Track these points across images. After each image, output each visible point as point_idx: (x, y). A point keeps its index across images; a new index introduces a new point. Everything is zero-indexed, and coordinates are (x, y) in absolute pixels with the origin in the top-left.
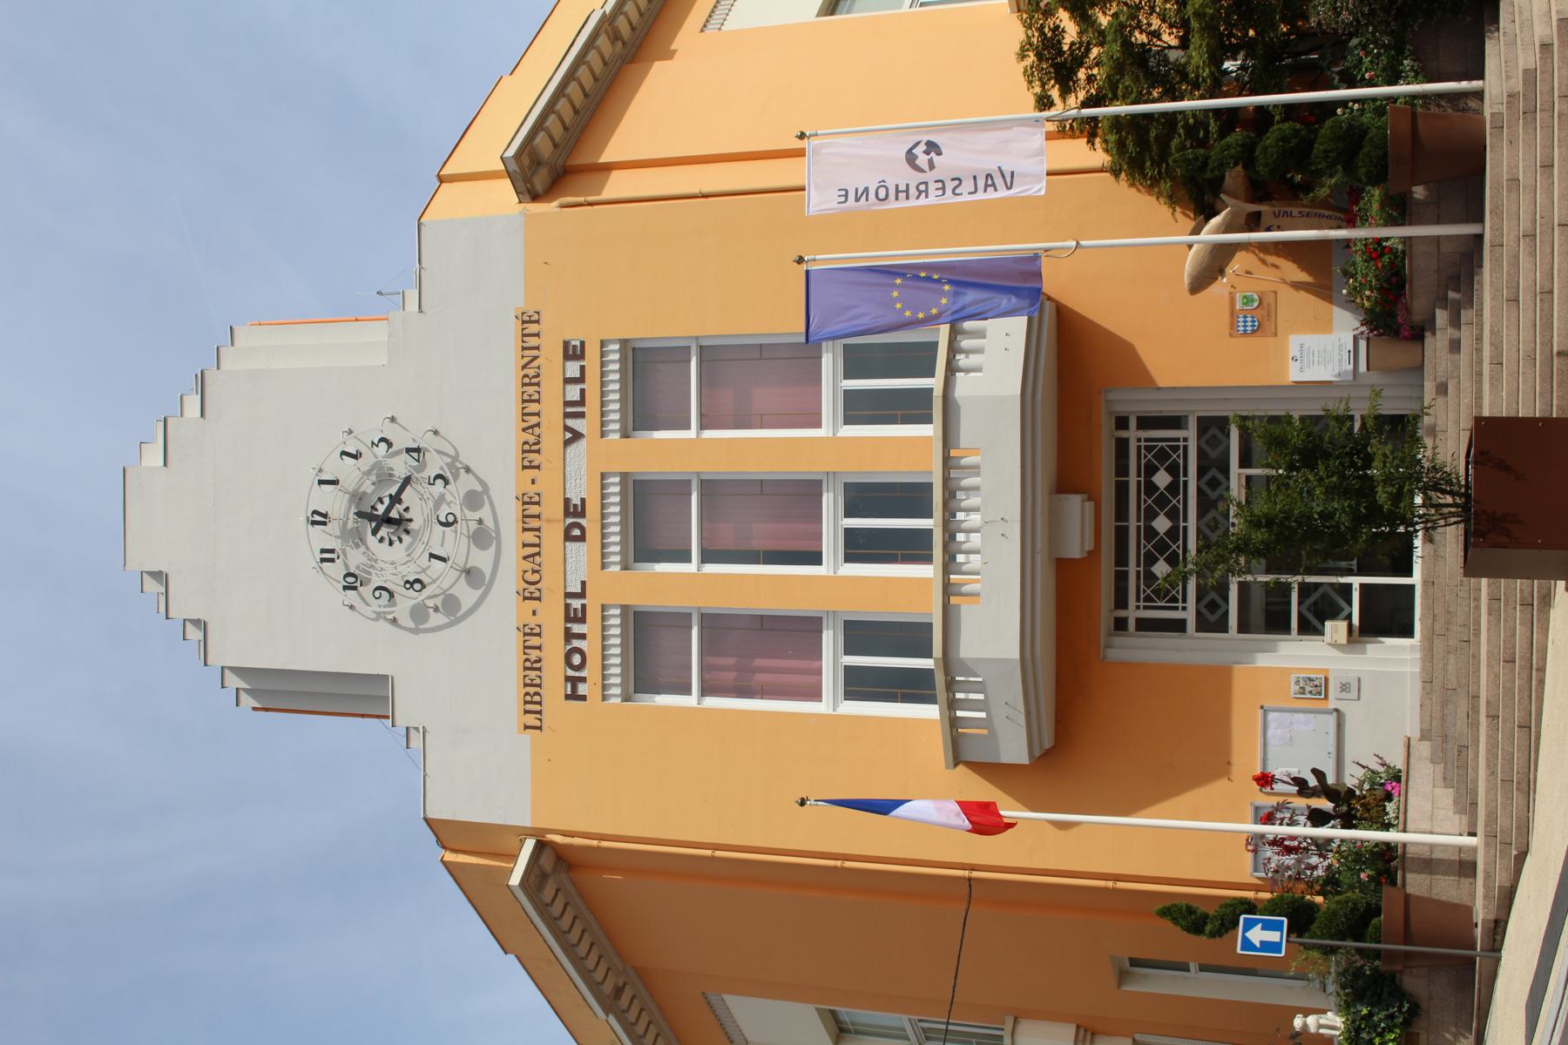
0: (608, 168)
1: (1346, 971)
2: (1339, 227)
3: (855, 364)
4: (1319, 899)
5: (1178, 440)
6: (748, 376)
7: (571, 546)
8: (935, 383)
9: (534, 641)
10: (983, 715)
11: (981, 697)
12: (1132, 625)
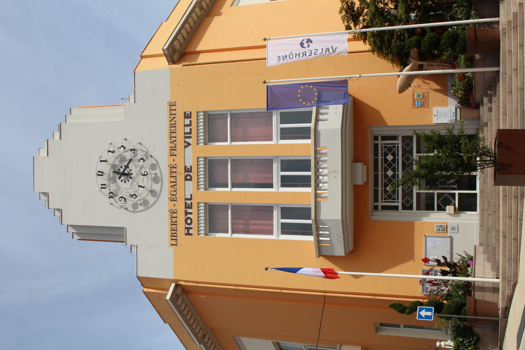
0: (199, 52)
1: (454, 326)
2: (450, 69)
3: (284, 119)
4: (445, 302)
5: (395, 144)
6: (246, 124)
7: (187, 182)
8: (312, 125)
9: (175, 215)
10: (329, 239)
11: (328, 233)
12: (380, 208)
